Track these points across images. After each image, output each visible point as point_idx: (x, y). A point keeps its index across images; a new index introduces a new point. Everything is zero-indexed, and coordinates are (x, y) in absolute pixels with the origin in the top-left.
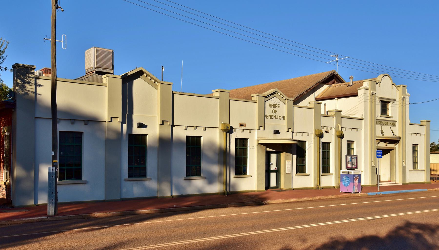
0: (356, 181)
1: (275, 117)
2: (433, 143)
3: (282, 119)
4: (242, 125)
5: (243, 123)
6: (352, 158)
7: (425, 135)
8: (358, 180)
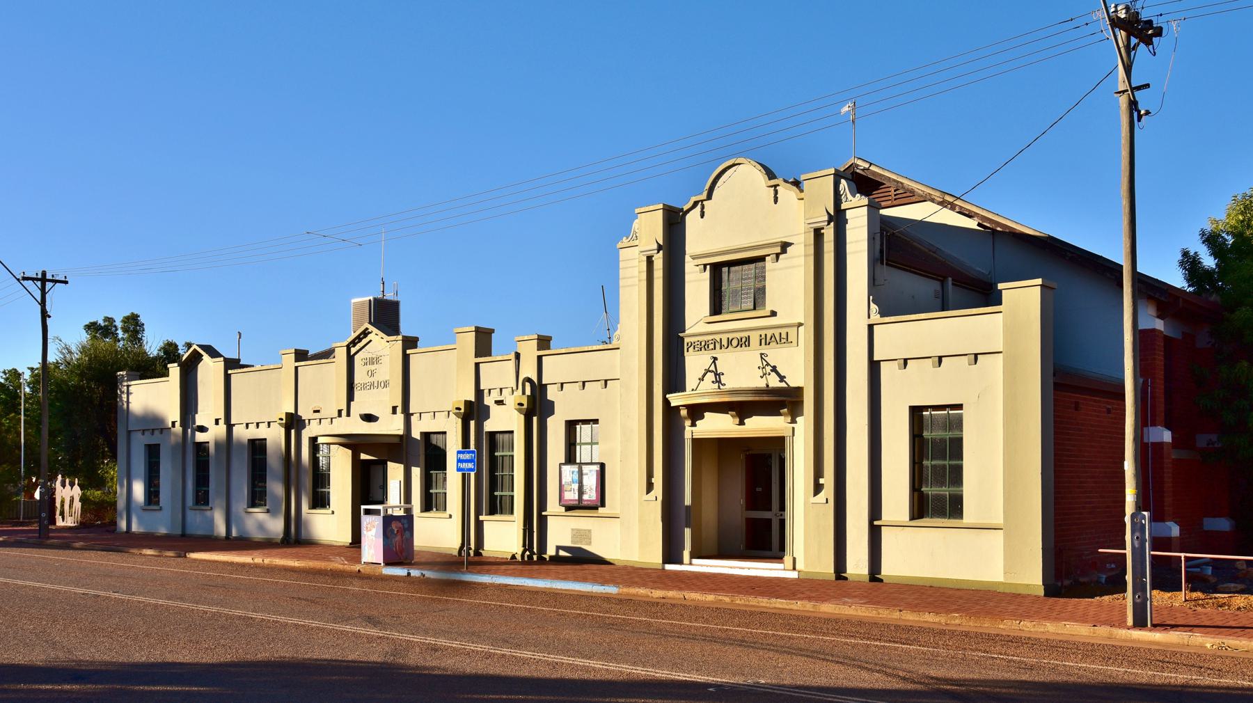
0: (370, 533)
1: (372, 385)
2: (520, 411)
3: (741, 347)
4: (315, 412)
6: (581, 474)
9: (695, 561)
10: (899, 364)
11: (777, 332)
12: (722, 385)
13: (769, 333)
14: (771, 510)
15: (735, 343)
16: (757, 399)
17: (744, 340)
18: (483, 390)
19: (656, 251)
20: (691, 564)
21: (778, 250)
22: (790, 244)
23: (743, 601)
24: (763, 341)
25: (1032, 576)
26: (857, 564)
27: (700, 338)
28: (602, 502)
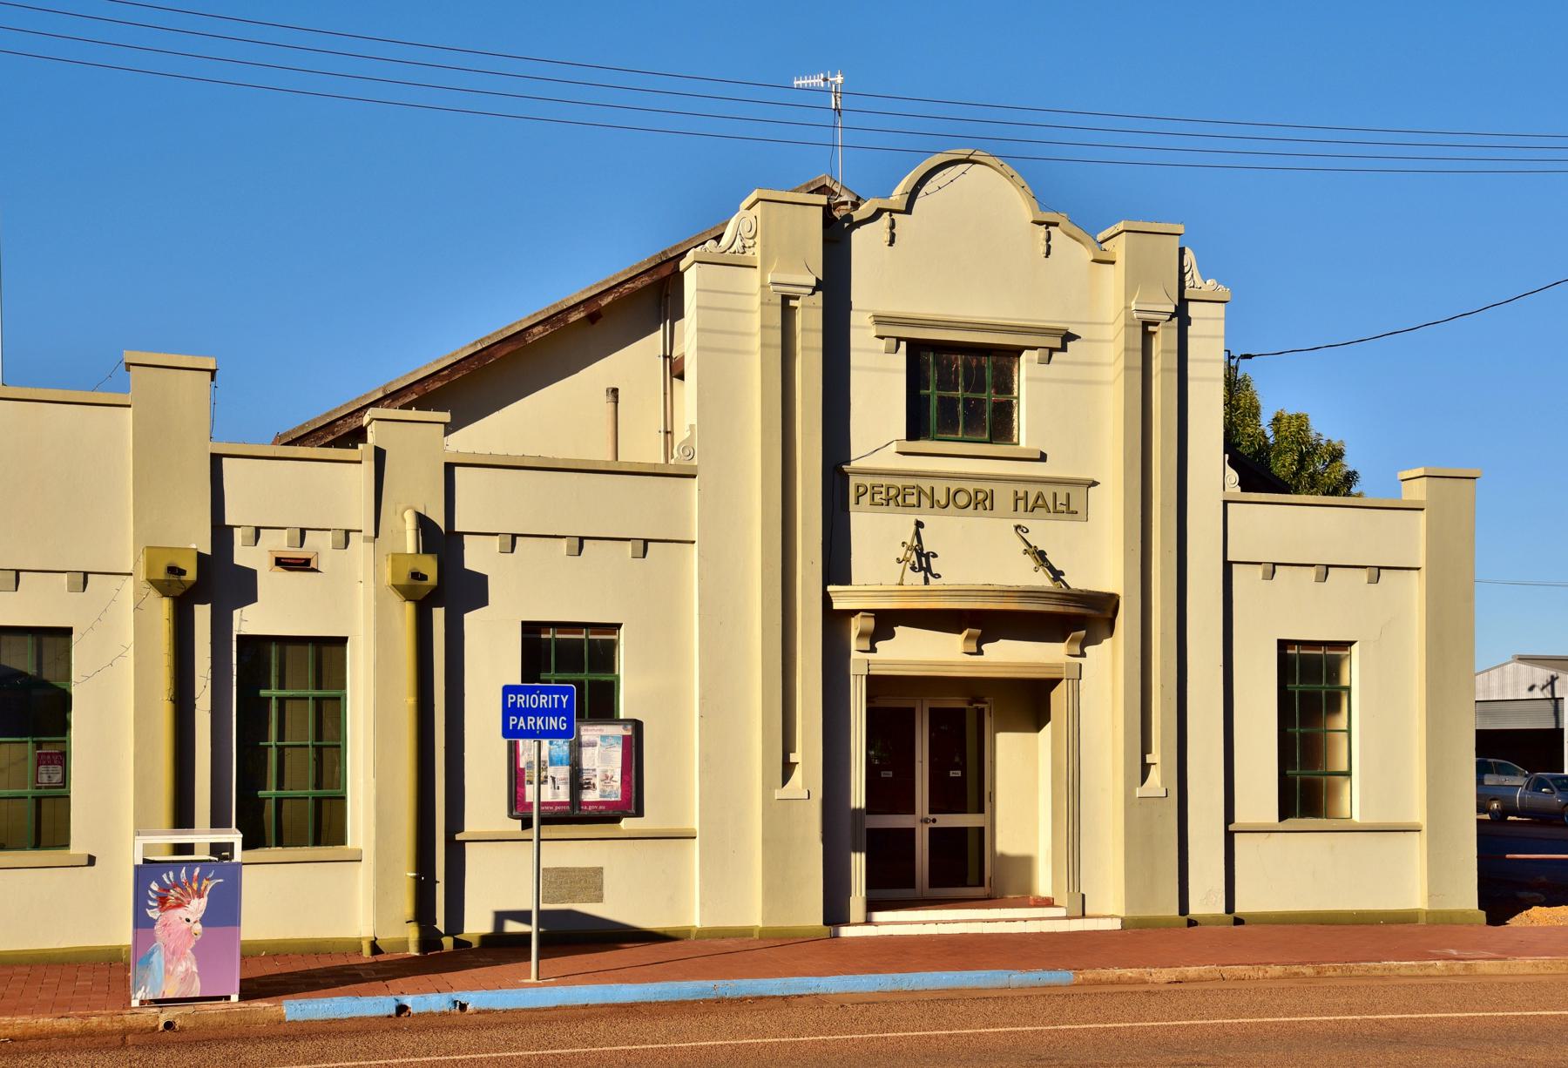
5: (1530, 685)
7: (1423, 571)
8: (197, 906)
9: (878, 916)
10: (1369, 575)
11: (1048, 492)
12: (934, 576)
13: (1033, 491)
14: (913, 812)
15: (962, 499)
16: (1060, 609)
17: (981, 496)
18: (231, 528)
19: (810, 291)
20: (868, 922)
21: (1057, 343)
22: (1073, 337)
23: (1339, 971)
24: (1021, 504)
25: (1465, 896)
26: (1206, 900)
27: (885, 481)
28: (633, 801)
